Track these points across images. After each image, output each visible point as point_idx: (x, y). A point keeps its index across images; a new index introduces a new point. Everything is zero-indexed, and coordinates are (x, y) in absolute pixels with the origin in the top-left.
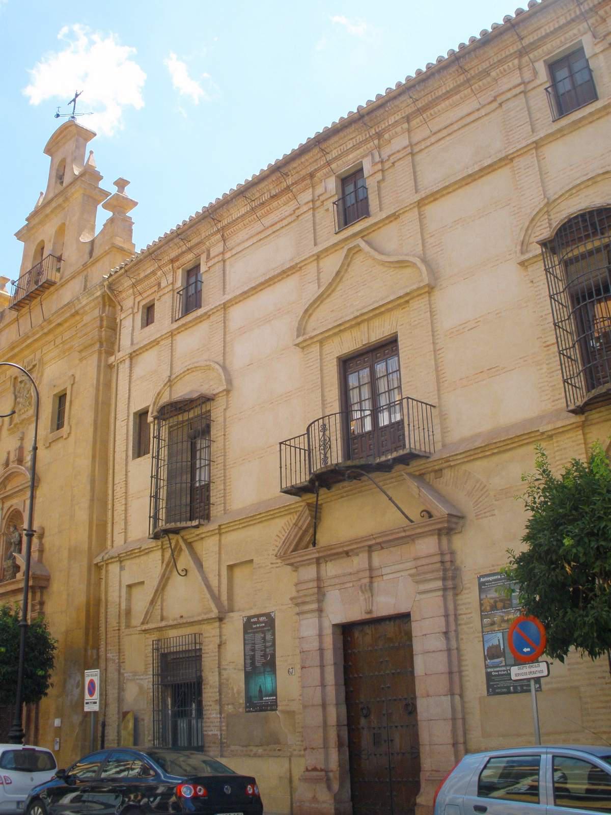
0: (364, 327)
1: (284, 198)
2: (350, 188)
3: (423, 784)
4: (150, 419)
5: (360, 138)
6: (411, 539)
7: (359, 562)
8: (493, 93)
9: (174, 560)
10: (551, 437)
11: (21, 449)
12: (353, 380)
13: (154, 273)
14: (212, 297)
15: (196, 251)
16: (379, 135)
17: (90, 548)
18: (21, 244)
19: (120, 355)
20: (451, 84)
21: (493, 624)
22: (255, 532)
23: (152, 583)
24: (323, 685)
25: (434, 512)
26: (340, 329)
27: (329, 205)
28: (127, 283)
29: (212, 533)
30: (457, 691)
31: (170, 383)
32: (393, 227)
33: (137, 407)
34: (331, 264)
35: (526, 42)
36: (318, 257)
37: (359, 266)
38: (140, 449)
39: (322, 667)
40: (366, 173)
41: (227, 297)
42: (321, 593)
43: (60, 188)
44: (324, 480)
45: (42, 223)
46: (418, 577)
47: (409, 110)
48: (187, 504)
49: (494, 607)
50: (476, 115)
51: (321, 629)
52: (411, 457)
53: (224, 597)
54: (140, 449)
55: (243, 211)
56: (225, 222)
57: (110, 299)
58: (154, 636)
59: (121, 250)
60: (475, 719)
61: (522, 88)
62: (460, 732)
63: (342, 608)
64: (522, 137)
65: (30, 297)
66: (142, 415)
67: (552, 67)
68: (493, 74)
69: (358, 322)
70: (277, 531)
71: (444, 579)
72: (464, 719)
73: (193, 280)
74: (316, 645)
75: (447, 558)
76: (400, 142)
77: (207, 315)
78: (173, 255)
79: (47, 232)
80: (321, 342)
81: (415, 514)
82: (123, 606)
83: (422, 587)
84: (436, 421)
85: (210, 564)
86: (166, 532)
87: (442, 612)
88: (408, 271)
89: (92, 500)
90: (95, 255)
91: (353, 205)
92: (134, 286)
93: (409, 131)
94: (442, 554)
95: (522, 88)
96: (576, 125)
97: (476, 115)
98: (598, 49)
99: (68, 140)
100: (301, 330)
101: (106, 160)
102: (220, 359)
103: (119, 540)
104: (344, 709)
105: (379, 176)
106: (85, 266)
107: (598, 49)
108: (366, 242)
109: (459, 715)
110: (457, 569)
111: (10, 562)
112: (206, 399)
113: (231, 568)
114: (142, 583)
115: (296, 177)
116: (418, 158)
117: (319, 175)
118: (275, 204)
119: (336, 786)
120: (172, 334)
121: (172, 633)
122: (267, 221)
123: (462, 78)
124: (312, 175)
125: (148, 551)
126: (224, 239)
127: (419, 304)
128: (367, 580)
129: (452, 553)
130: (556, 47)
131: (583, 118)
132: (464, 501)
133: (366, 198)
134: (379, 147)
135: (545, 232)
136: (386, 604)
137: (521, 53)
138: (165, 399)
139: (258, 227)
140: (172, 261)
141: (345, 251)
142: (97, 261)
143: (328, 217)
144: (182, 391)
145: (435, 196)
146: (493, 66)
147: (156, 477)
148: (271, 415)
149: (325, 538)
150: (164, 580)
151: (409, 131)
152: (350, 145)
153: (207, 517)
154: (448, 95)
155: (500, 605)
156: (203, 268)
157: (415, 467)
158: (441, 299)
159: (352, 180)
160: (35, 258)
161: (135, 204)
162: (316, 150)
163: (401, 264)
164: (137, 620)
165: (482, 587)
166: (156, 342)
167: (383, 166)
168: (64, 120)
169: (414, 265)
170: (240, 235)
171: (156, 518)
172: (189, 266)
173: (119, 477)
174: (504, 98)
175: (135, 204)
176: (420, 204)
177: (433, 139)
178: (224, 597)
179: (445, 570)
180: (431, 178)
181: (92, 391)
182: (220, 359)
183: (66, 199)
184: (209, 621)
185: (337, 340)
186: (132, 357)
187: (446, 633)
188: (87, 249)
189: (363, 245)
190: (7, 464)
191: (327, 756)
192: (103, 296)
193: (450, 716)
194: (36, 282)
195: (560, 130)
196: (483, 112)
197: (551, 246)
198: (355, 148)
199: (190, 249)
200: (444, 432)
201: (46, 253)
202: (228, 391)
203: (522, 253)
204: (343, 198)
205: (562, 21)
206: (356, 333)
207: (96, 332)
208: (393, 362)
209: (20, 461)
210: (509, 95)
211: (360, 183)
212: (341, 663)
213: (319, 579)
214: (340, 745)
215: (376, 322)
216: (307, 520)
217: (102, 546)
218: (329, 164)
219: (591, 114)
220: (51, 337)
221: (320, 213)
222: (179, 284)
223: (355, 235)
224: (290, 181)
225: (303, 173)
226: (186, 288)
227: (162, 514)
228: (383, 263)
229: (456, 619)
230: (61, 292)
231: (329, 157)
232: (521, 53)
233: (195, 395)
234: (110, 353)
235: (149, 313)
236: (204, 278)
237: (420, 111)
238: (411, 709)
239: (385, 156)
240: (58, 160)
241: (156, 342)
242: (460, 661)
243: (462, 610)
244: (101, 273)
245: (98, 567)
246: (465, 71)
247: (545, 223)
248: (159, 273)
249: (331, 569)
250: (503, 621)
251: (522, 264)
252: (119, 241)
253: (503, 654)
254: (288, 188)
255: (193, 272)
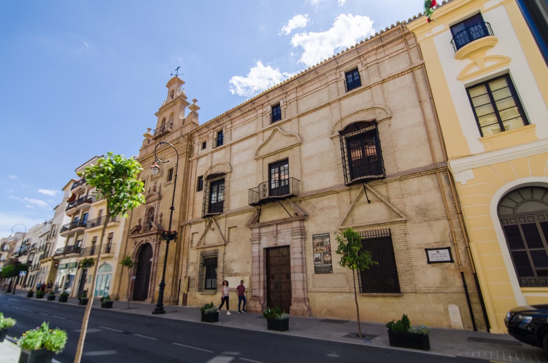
0: (278, 155)
1: (253, 112)
2: (275, 110)
3: (292, 302)
4: (203, 179)
5: (280, 93)
6: (291, 222)
7: (273, 228)
8: (326, 82)
9: (210, 224)
10: (338, 193)
11: (155, 187)
12: (273, 170)
13: (206, 132)
14: (227, 141)
15: (222, 126)
16: (286, 93)
17: (179, 221)
18: (157, 118)
19: (193, 158)
20: (312, 77)
21: (317, 250)
22: (238, 217)
23: (202, 232)
24: (259, 268)
25: (299, 214)
26: (269, 155)
27: (268, 115)
28: (197, 134)
29: (223, 217)
30: (305, 271)
31: (211, 168)
32: (289, 123)
33: (199, 175)
34: (268, 134)
35: (339, 65)
36: (263, 131)
37: (277, 134)
38: (199, 188)
39: (259, 262)
40: (281, 105)
41: (232, 142)
42: (260, 238)
43: (171, 100)
44: (262, 202)
45: (165, 110)
46: (293, 234)
47: (297, 85)
48: (214, 210)
49: (317, 245)
50: (319, 89)
51: (259, 249)
52: (293, 196)
53: (227, 238)
54: (199, 188)
55: (239, 114)
56: (232, 117)
57: (190, 138)
58: (201, 250)
59: (194, 123)
60: (310, 282)
61: (336, 80)
62: (305, 286)
63: (266, 243)
64: (335, 97)
65: (160, 136)
66: (200, 178)
67: (347, 74)
68: (327, 75)
69: (276, 153)
70: (246, 217)
71: (302, 235)
72: (307, 281)
73: (220, 135)
74: (257, 254)
75: (303, 228)
76: (293, 96)
77: (225, 147)
78: (214, 126)
79: (167, 114)
80: (263, 158)
81: (292, 215)
82: (190, 239)
83: (294, 237)
84: (300, 186)
85: (222, 227)
86: (207, 216)
87: (300, 246)
88: (293, 138)
89: (181, 205)
90: (185, 124)
91: (276, 114)
92: (199, 135)
93: (296, 92)
94: (301, 227)
95: (336, 80)
96: (353, 94)
97: (319, 89)
98: (363, 69)
99: (175, 82)
100: (257, 154)
101: (188, 91)
102: (229, 161)
103: (190, 218)
104: (266, 276)
105: (285, 107)
106: (181, 128)
107: (363, 69)
108: (281, 128)
109: (305, 280)
110: (305, 232)
111: (149, 224)
112: (223, 174)
113: (229, 228)
114: (198, 232)
115: (257, 105)
116: (299, 101)
117: (265, 105)
118: (249, 113)
119: (262, 302)
120: (212, 152)
121: (208, 249)
122: (247, 118)
123: (316, 75)
124: (263, 105)
125: (201, 222)
126: (231, 123)
127: (296, 149)
128: (275, 234)
129: (304, 227)
130: (349, 67)
131: (356, 92)
132: (308, 210)
133: (280, 114)
134: (286, 97)
135: (340, 128)
136: (281, 242)
137: (337, 68)
138: (209, 173)
139: (243, 120)
140: (213, 129)
141: (272, 130)
142: (186, 126)
143: (267, 119)
144: (214, 171)
145: (303, 114)
146: (327, 72)
147: (205, 198)
148: (245, 180)
149: (261, 220)
150: (206, 232)
151: (296, 92)
152: (276, 95)
153: (222, 211)
154: (311, 81)
155: (319, 244)
156: (224, 132)
157: (293, 199)
158: (303, 147)
159: (276, 108)
160: (162, 123)
161: (199, 108)
162: (265, 96)
163: (291, 136)
164: (195, 245)
165: (314, 238)
166: (206, 155)
167: (287, 103)
168: (173, 76)
169: (295, 136)
170: (237, 123)
171: (204, 211)
172: (219, 131)
173: (191, 197)
174: (329, 83)
175: (199, 108)
176: (299, 117)
177: (304, 96)
178: (227, 238)
179: (302, 232)
180: (303, 108)
181: (183, 169)
182: (229, 161)
183: (175, 104)
184: (221, 245)
185: (268, 158)
186: (198, 159)
187: (301, 253)
188: (182, 122)
189: (279, 129)
190: (149, 191)
191: (260, 292)
192: (188, 138)
193: (302, 280)
194: (163, 131)
195: (348, 95)
196: (322, 87)
197: (341, 133)
198: (278, 96)
199: (220, 125)
200: (303, 189)
201: (167, 121)
202: (231, 172)
203: (332, 135)
204: (273, 113)
205: (352, 58)
206: (275, 156)
207: (185, 150)
208: (286, 166)
209: (155, 190)
210: (331, 82)
211: (278, 109)
212: (265, 260)
213: (259, 233)
214: (264, 288)
215: (282, 154)
216: (256, 214)
217: (184, 219)
218: (269, 101)
219: (359, 90)
220: (168, 150)
221: (265, 117)
222: (215, 136)
223: (276, 125)
224: (255, 106)
225: (260, 104)
226: (218, 138)
227: (206, 210)
228: (285, 135)
229: (305, 248)
230: (173, 135)
231: (269, 99)
232: (337, 68)
233: (220, 173)
234: (190, 157)
235: (204, 146)
236: (224, 135)
237: (301, 86)
238: (288, 276)
239: (287, 100)
240: (171, 90)
241: (206, 155)
242: (306, 262)
243: (307, 245)
244: (188, 130)
245: (182, 227)
246: (317, 73)
247: (340, 125)
248: (208, 132)
249: (264, 230)
250: (320, 250)
251: (331, 138)
252: (194, 120)
253: (320, 261)
254: (254, 108)
255: (220, 133)
